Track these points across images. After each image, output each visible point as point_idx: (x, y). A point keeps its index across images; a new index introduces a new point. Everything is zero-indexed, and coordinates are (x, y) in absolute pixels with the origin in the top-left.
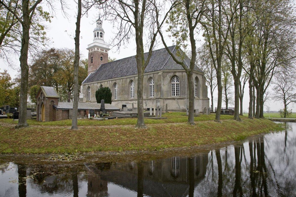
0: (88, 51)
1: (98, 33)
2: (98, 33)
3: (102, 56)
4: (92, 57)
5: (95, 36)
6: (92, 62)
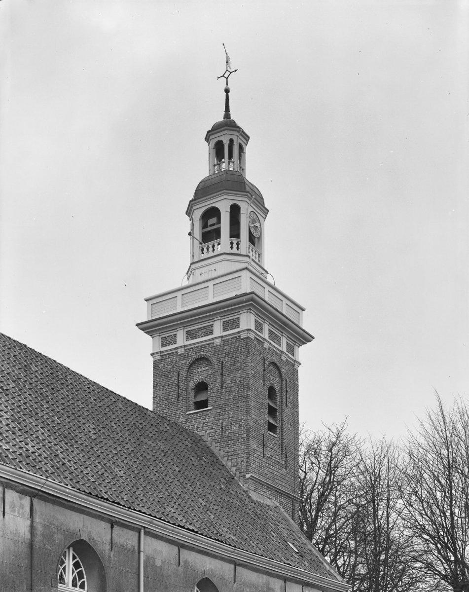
0: (148, 344)
1: (235, 211)
5: (209, 235)
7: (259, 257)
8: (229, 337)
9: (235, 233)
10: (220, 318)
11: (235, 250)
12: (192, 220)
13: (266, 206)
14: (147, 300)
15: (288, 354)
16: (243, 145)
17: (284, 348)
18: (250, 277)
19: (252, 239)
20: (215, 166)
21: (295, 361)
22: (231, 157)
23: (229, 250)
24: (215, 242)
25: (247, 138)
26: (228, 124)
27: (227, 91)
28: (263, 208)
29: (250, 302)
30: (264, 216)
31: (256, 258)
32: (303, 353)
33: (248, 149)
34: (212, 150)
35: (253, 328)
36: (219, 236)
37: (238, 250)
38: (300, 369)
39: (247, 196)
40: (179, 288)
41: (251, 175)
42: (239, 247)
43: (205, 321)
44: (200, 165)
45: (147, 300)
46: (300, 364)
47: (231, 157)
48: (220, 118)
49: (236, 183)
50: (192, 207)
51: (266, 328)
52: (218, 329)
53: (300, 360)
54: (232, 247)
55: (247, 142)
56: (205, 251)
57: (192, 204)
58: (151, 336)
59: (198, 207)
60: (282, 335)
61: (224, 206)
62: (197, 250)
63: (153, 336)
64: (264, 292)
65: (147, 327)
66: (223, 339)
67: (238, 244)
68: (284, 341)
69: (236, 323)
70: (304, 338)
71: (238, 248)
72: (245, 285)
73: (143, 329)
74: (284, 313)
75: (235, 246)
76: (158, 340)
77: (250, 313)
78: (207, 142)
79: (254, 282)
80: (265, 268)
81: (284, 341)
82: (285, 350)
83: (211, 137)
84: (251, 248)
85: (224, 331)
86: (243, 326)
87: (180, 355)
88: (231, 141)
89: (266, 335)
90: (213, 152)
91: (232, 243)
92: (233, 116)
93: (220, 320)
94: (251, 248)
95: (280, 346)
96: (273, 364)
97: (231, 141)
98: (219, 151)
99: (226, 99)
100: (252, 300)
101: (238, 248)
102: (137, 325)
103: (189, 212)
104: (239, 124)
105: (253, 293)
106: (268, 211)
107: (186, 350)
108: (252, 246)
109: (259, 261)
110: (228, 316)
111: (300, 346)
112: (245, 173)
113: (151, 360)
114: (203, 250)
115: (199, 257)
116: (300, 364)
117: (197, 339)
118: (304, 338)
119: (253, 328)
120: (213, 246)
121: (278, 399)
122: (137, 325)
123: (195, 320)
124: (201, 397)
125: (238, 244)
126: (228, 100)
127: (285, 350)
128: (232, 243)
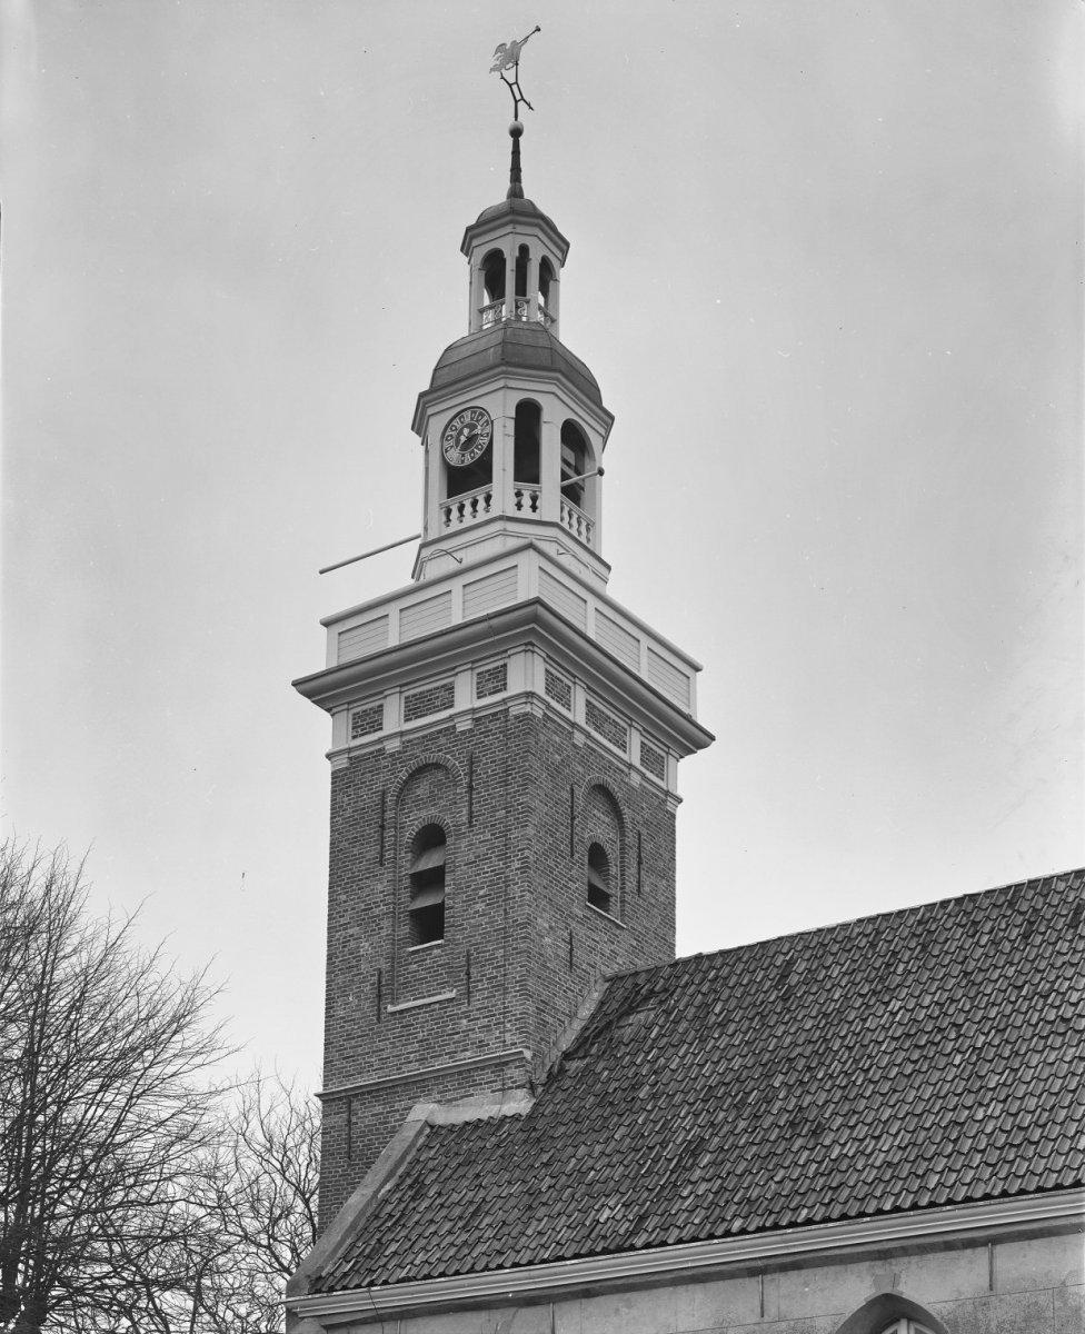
0: (320, 730)
1: (528, 416)
2: (528, 416)
3: (599, 828)
4: (432, 837)
5: (464, 478)
6: (430, 924)
7: (588, 530)
8: (416, 735)
9: (527, 467)
10: (469, 666)
11: (526, 513)
12: (424, 442)
13: (605, 404)
14: (327, 624)
15: (644, 770)
16: (555, 263)
17: (634, 756)
18: (649, 649)
19: (572, 493)
20: (482, 311)
21: (667, 793)
22: (521, 289)
23: (512, 512)
24: (480, 495)
25: (563, 246)
26: (518, 211)
27: (516, 133)
28: (597, 410)
29: (531, 626)
30: (603, 432)
31: (571, 526)
32: (688, 774)
33: (565, 275)
34: (476, 273)
35: (541, 691)
36: (488, 479)
37: (534, 511)
38: (681, 813)
39: (558, 380)
40: (388, 597)
41: (571, 336)
42: (538, 503)
43: (419, 680)
44: (446, 308)
45: (327, 624)
46: (680, 801)
47: (521, 289)
48: (498, 196)
49: (530, 353)
50: (425, 409)
51: (580, 697)
52: (465, 696)
53: (680, 792)
54: (519, 506)
55: (608, 432)
56: (455, 514)
57: (425, 400)
58: (328, 710)
59: (436, 409)
60: (630, 726)
61: (500, 407)
62: (437, 516)
63: (335, 710)
64: (639, 649)
65: (318, 690)
66: (352, 755)
67: (534, 499)
68: (635, 740)
69: (498, 678)
70: (693, 739)
71: (534, 508)
72: (527, 582)
73: (308, 694)
74: (592, 635)
75: (527, 501)
76: (346, 719)
77: (533, 652)
78: (467, 255)
79: (658, 660)
80: (699, 722)
81: (635, 740)
82: (636, 762)
83: (475, 243)
84: (566, 509)
85: (406, 721)
86: (516, 683)
87: (392, 755)
88: (524, 250)
89: (579, 714)
90: (480, 278)
91: (519, 494)
92: (530, 192)
93: (470, 672)
94: (566, 509)
95: (625, 751)
96: (602, 790)
97: (524, 250)
98: (492, 273)
99: (513, 153)
100: (536, 619)
101: (534, 508)
102: (295, 684)
103: (419, 425)
104: (544, 208)
105: (538, 601)
106: (612, 418)
107: (477, 720)
108: (569, 504)
109: (589, 540)
110: (488, 661)
111: (682, 757)
112: (557, 330)
113: (327, 768)
114: (449, 512)
115: (440, 533)
116: (680, 801)
117: (413, 722)
118: (693, 739)
119: (541, 691)
120: (474, 504)
121: (614, 870)
122: (295, 684)
123: (420, 667)
124: (430, 862)
125: (534, 499)
126: (519, 153)
127: (636, 762)
128: (519, 494)
